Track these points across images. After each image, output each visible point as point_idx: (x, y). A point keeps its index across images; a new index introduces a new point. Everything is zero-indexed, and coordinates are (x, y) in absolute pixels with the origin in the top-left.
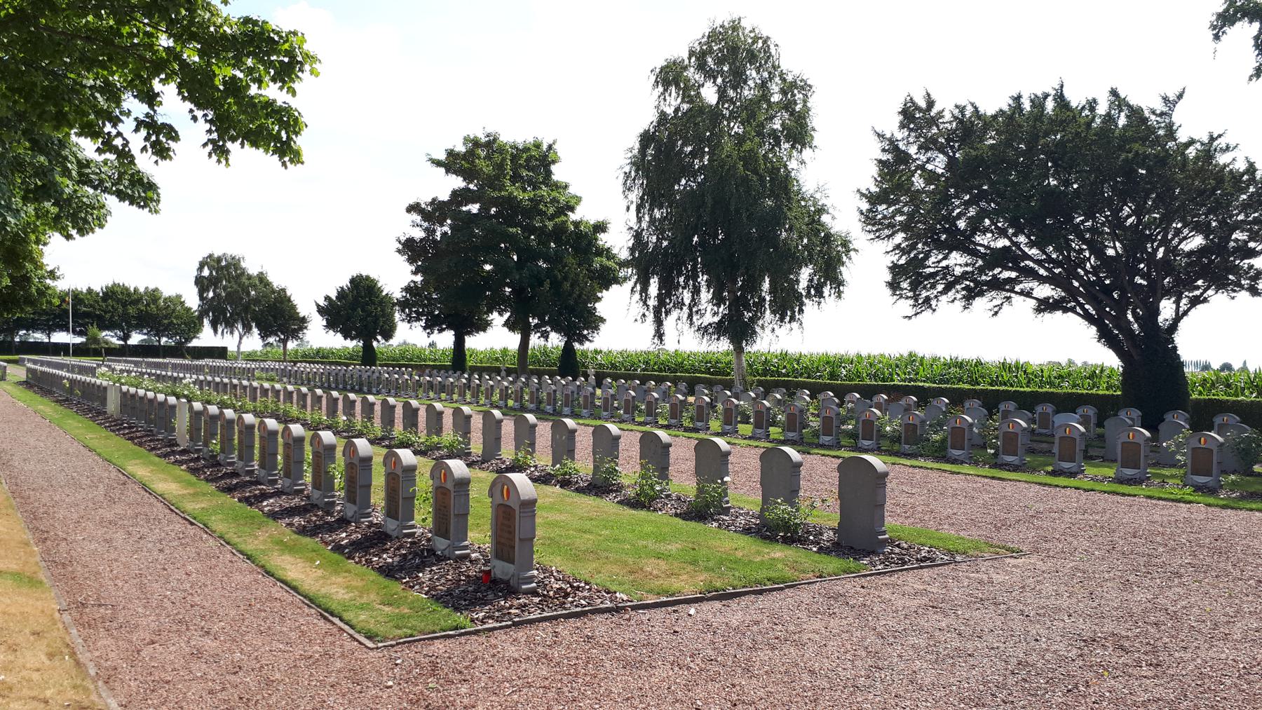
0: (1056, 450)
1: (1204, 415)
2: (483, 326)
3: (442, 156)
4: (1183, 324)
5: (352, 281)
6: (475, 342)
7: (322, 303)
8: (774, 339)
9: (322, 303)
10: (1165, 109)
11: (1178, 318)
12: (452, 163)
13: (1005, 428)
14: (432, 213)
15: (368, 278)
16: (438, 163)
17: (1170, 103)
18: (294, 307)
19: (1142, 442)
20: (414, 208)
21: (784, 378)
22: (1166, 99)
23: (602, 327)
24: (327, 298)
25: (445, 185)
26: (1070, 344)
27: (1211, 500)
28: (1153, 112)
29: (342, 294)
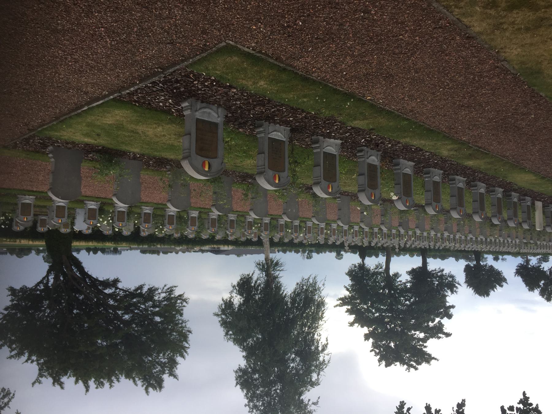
0: (66, 210)
1: (31, 233)
2: (413, 272)
3: (433, 361)
4: (45, 274)
5: (488, 295)
6: (416, 262)
7: (504, 284)
8: (248, 265)
9: (504, 284)
10: (40, 379)
11: (47, 276)
12: (427, 358)
13: (95, 222)
14: (437, 331)
15: (480, 295)
16: (434, 358)
17: (38, 381)
18: (524, 281)
19: (20, 216)
20: (448, 335)
21: (243, 246)
22: (40, 382)
23: (347, 271)
24: (502, 286)
25: (432, 346)
26: (98, 265)
27: (104, 201)
28: (45, 377)
29: (493, 288)
